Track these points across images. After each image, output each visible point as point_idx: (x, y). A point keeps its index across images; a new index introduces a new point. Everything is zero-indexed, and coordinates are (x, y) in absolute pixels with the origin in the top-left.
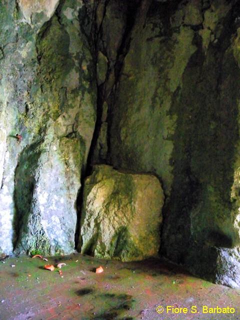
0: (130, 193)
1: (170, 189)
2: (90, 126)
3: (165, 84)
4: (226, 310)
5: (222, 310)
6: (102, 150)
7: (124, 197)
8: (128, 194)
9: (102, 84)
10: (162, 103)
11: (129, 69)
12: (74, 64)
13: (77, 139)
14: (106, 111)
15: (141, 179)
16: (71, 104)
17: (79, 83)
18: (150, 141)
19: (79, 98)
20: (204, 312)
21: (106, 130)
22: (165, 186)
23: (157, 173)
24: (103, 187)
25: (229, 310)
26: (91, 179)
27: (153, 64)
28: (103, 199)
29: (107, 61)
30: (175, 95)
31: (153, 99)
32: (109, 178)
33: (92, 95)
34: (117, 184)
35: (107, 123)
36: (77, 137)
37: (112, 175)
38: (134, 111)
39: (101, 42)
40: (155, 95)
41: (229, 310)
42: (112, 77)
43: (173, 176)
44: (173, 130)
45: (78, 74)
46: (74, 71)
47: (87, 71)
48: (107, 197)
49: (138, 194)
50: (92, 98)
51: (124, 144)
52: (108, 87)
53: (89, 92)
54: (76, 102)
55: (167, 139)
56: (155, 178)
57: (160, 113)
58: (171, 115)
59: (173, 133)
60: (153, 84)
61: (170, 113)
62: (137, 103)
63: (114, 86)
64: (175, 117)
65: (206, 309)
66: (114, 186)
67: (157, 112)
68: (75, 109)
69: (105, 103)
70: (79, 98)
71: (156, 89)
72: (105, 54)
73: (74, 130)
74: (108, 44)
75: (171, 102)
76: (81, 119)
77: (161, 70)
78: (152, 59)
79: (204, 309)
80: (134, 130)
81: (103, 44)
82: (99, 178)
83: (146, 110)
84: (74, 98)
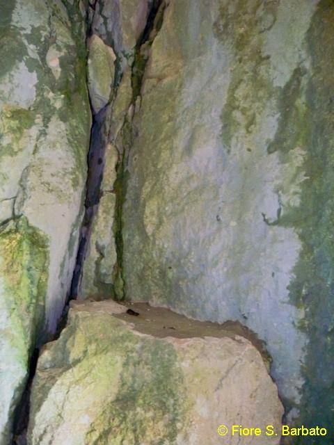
0: (171, 401)
1: (301, 383)
2: (60, 195)
3: (255, 72)
4: (314, 431)
5: (309, 431)
6: (103, 261)
7: (150, 414)
8: (163, 407)
9: (103, 110)
10: (252, 122)
11: (161, 64)
12: (22, 51)
13: (18, 236)
14: (113, 166)
15: (204, 354)
16: (10, 145)
17: (37, 95)
18: (224, 232)
19: (34, 131)
20: (284, 434)
21: (112, 212)
22: (279, 370)
23: (251, 326)
24: (88, 379)
25: (319, 431)
26: (56, 350)
27: (218, 35)
28: (86, 420)
29: (115, 58)
30: (287, 97)
31: (226, 118)
32: (105, 350)
33: (71, 125)
34: (131, 368)
35: (114, 195)
36: (21, 230)
37: (115, 341)
38: (177, 155)
39: (102, 20)
40: (231, 106)
41: (319, 431)
42: (125, 88)
43: (305, 340)
44: (295, 193)
45: (34, 74)
46: (22, 65)
47: (60, 70)
48: (100, 410)
49: (196, 408)
50: (73, 134)
51: (154, 243)
52: (118, 111)
53: (63, 118)
54: (23, 142)
55: (277, 223)
56: (249, 347)
57: (249, 150)
58: (285, 151)
59: (296, 202)
60: (223, 80)
61: (278, 145)
62: (184, 133)
63: (131, 108)
64: (299, 155)
65: (287, 430)
66: (121, 375)
67: (240, 146)
68: (20, 156)
69: (109, 147)
70: (34, 131)
71: (233, 89)
72: (110, 42)
73: (16, 213)
74: (116, 21)
75: (278, 115)
76: (32, 180)
77: (240, 43)
78: (216, 24)
79: (284, 430)
80: (178, 204)
81: (105, 23)
82: (74, 354)
83: (207, 150)
84: (19, 129)
